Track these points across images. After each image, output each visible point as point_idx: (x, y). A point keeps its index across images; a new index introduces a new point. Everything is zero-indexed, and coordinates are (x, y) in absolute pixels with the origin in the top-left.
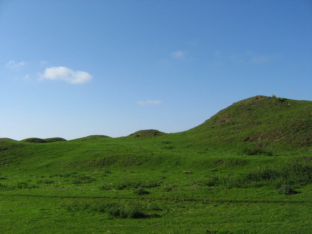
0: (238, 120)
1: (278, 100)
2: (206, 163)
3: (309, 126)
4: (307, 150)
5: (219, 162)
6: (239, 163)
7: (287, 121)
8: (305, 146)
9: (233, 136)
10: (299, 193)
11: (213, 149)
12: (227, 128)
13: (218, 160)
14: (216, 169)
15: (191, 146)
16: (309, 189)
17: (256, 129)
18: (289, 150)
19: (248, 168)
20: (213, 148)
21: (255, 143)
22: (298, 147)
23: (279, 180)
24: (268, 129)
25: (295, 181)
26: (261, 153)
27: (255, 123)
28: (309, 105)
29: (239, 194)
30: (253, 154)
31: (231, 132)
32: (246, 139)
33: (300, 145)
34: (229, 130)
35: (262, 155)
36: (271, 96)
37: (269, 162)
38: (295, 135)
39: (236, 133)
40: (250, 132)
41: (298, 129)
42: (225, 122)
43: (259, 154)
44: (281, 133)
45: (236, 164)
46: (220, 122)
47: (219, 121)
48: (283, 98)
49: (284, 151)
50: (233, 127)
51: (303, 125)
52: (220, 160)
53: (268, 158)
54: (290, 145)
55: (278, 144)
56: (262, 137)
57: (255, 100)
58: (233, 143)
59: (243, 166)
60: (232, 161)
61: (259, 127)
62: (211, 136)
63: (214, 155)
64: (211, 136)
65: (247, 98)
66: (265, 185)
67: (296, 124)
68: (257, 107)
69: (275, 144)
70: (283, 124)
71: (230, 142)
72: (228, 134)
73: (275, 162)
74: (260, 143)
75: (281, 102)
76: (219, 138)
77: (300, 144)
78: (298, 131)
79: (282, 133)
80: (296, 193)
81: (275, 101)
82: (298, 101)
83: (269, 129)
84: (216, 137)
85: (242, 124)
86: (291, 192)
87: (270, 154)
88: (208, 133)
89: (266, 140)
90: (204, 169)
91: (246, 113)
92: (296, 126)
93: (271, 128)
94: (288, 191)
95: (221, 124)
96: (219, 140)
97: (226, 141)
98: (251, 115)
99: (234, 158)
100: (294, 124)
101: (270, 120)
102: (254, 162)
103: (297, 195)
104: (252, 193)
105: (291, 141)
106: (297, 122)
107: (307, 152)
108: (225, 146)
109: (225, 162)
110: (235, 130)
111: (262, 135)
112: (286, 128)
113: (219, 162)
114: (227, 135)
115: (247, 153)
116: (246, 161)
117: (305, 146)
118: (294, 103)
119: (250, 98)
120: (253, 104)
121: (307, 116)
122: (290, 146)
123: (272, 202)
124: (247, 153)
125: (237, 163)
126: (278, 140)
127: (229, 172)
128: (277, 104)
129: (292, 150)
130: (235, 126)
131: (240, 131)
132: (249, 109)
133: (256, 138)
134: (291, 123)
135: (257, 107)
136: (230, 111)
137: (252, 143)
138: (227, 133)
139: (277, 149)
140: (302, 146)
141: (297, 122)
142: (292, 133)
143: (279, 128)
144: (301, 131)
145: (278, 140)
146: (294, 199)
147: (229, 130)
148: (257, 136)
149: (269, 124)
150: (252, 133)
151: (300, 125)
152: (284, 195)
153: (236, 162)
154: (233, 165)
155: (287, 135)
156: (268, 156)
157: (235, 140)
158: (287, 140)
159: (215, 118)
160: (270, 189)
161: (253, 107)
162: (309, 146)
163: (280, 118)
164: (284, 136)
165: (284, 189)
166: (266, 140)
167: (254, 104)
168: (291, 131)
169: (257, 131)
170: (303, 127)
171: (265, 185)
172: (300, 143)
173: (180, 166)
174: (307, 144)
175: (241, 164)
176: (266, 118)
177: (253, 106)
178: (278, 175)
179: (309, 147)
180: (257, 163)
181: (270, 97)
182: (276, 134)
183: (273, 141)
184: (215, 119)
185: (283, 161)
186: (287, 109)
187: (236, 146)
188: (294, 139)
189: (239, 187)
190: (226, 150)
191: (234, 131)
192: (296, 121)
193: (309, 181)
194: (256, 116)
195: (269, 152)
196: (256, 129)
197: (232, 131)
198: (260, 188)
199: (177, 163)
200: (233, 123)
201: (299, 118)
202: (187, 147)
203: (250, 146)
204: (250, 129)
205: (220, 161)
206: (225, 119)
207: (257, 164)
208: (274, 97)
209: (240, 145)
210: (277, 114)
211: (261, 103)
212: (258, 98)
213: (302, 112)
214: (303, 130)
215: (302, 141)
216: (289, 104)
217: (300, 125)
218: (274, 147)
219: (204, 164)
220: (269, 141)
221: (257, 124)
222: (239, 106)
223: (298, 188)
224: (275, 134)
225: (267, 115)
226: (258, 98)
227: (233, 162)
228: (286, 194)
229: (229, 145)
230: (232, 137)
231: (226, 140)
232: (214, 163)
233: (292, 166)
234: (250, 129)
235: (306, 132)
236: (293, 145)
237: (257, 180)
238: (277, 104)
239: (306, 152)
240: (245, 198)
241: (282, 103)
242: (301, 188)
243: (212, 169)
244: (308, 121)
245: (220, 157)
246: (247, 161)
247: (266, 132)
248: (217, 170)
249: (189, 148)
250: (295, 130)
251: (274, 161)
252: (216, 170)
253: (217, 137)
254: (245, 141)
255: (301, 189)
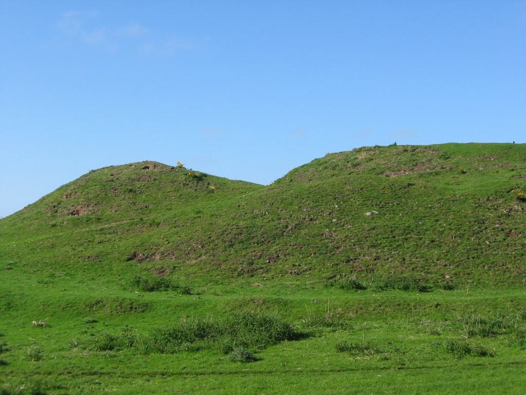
0: (108, 213)
1: (190, 176)
2: (71, 307)
3: (253, 237)
4: (249, 283)
5: (96, 304)
6: (136, 308)
7: (211, 224)
8: (246, 275)
9: (100, 248)
10: (261, 359)
11: (65, 275)
12: (87, 229)
13: (94, 302)
14: (93, 319)
15: (16, 266)
16: (273, 354)
17: (150, 237)
18: (217, 283)
19: (154, 317)
20: (65, 273)
21: (150, 266)
22: (233, 277)
23: (226, 340)
24: (173, 239)
25: (249, 342)
26: (168, 287)
27: (145, 223)
28: (251, 193)
29: (160, 362)
30: (152, 290)
31: (97, 241)
32: (130, 257)
33: (236, 274)
34: (92, 235)
35: (171, 293)
36: (175, 165)
37: (190, 308)
38: (227, 253)
39: (108, 241)
40: (138, 242)
41: (232, 242)
42: (78, 214)
43: (164, 290)
44: (200, 247)
45: (131, 310)
46: (68, 214)
47: (66, 212)
48: (201, 173)
49: (207, 284)
50: (99, 229)
51: (241, 234)
52: (100, 301)
53: (186, 299)
54: (218, 272)
55: (195, 270)
56: (163, 254)
57: (143, 171)
58: (104, 263)
59: (143, 314)
60: (121, 303)
61: (155, 231)
62: (53, 246)
63: (80, 290)
64: (53, 246)
65: (123, 163)
66: (204, 348)
67: (228, 232)
68: (147, 188)
69: (191, 270)
70: (203, 229)
71: (97, 260)
72: (90, 243)
73: (200, 307)
74: (160, 266)
75: (196, 182)
76: (74, 252)
77: (236, 272)
78: (231, 246)
79: (202, 247)
80: (256, 360)
81: (184, 177)
82: (229, 180)
83: (175, 238)
84: (65, 249)
85: (118, 223)
86: (249, 359)
87: (187, 292)
88: (47, 238)
89: (171, 261)
90: (69, 318)
91: (123, 199)
92: (228, 234)
93: (180, 237)
94: (244, 357)
95: (73, 220)
96: (74, 255)
97: (89, 257)
98: (134, 204)
99: (124, 299)
100: (223, 231)
101: (176, 219)
102: (163, 307)
103: (259, 363)
104: (187, 360)
105: (220, 265)
106: (230, 228)
107: (251, 288)
108: (88, 269)
109: (108, 305)
110: (105, 234)
111: (162, 249)
112: (210, 238)
113: (96, 304)
114: (89, 245)
115: (141, 287)
116: (147, 304)
117: (246, 275)
118: (222, 184)
119: (131, 165)
120: (139, 181)
121: (249, 215)
122: (218, 275)
123: (226, 374)
124: (141, 287)
125: (131, 308)
126: (194, 262)
127: (120, 323)
128: (187, 185)
129: (222, 283)
130: (104, 227)
131: (116, 238)
132: (131, 191)
133: (152, 255)
134: (219, 229)
135: (147, 188)
136: (87, 190)
137: (144, 265)
138: (90, 241)
139: (195, 280)
140: (239, 275)
141: (230, 228)
142: (221, 250)
143: (196, 237)
144: (238, 246)
145: (194, 262)
146: (258, 369)
147: (92, 235)
148: (153, 251)
149: (175, 227)
150: (142, 244)
151: (235, 235)
152: (239, 363)
153: (130, 306)
154: (125, 312)
155: (211, 252)
156: (184, 295)
157: (108, 256)
158: (213, 263)
159: (54, 204)
160: (214, 354)
161: (138, 186)
162: (252, 276)
163: (197, 216)
164: (206, 253)
165: (239, 354)
166: (171, 261)
167: (141, 180)
168: (219, 245)
169: (152, 241)
170: (241, 237)
171: (204, 348)
172: (235, 270)
173: (17, 310)
174: (248, 272)
175: (140, 310)
176: (169, 214)
177: (138, 184)
178: (221, 333)
179: (483, 358)
180: (168, 308)
181: (173, 168)
182: (190, 250)
183: (184, 262)
184: (54, 207)
185: (215, 306)
186: (209, 197)
187: (111, 269)
188: (224, 261)
189: (162, 352)
190: (93, 279)
191: (102, 238)
192: (228, 225)
193: (269, 342)
194: (146, 207)
195: (185, 287)
196: (150, 237)
197: (98, 238)
198: (196, 352)
199: (9, 306)
200: (99, 219)
201: (233, 219)
202: (9, 269)
203: (147, 271)
204: (135, 235)
205: (98, 302)
206: (79, 207)
207: (169, 312)
208: (181, 167)
209: (120, 268)
210: (189, 207)
211: (155, 180)
212: (148, 168)
213: (239, 206)
214: (241, 244)
215: (240, 266)
216: (212, 187)
217: (235, 235)
218: (187, 275)
219: (67, 307)
220: (178, 264)
221: (151, 225)
222: (107, 181)
223: (255, 353)
224: (189, 248)
225: (169, 207)
226: (148, 168)
227: (123, 305)
228: (242, 361)
229: (96, 267)
230: (101, 250)
231: (89, 255)
232: (86, 306)
233: (241, 318)
234: (135, 235)
235: (246, 248)
236: (223, 272)
237: (186, 338)
238: (187, 185)
239: (248, 288)
240: (183, 369)
241: (198, 183)
242: (260, 352)
243: (86, 319)
244: (251, 227)
245: (97, 295)
246: (149, 305)
247: (171, 244)
248: (96, 319)
249: (13, 271)
250: (227, 244)
251: (198, 305)
252: (94, 321)
253: (68, 248)
254: (129, 260)
255: (261, 354)
